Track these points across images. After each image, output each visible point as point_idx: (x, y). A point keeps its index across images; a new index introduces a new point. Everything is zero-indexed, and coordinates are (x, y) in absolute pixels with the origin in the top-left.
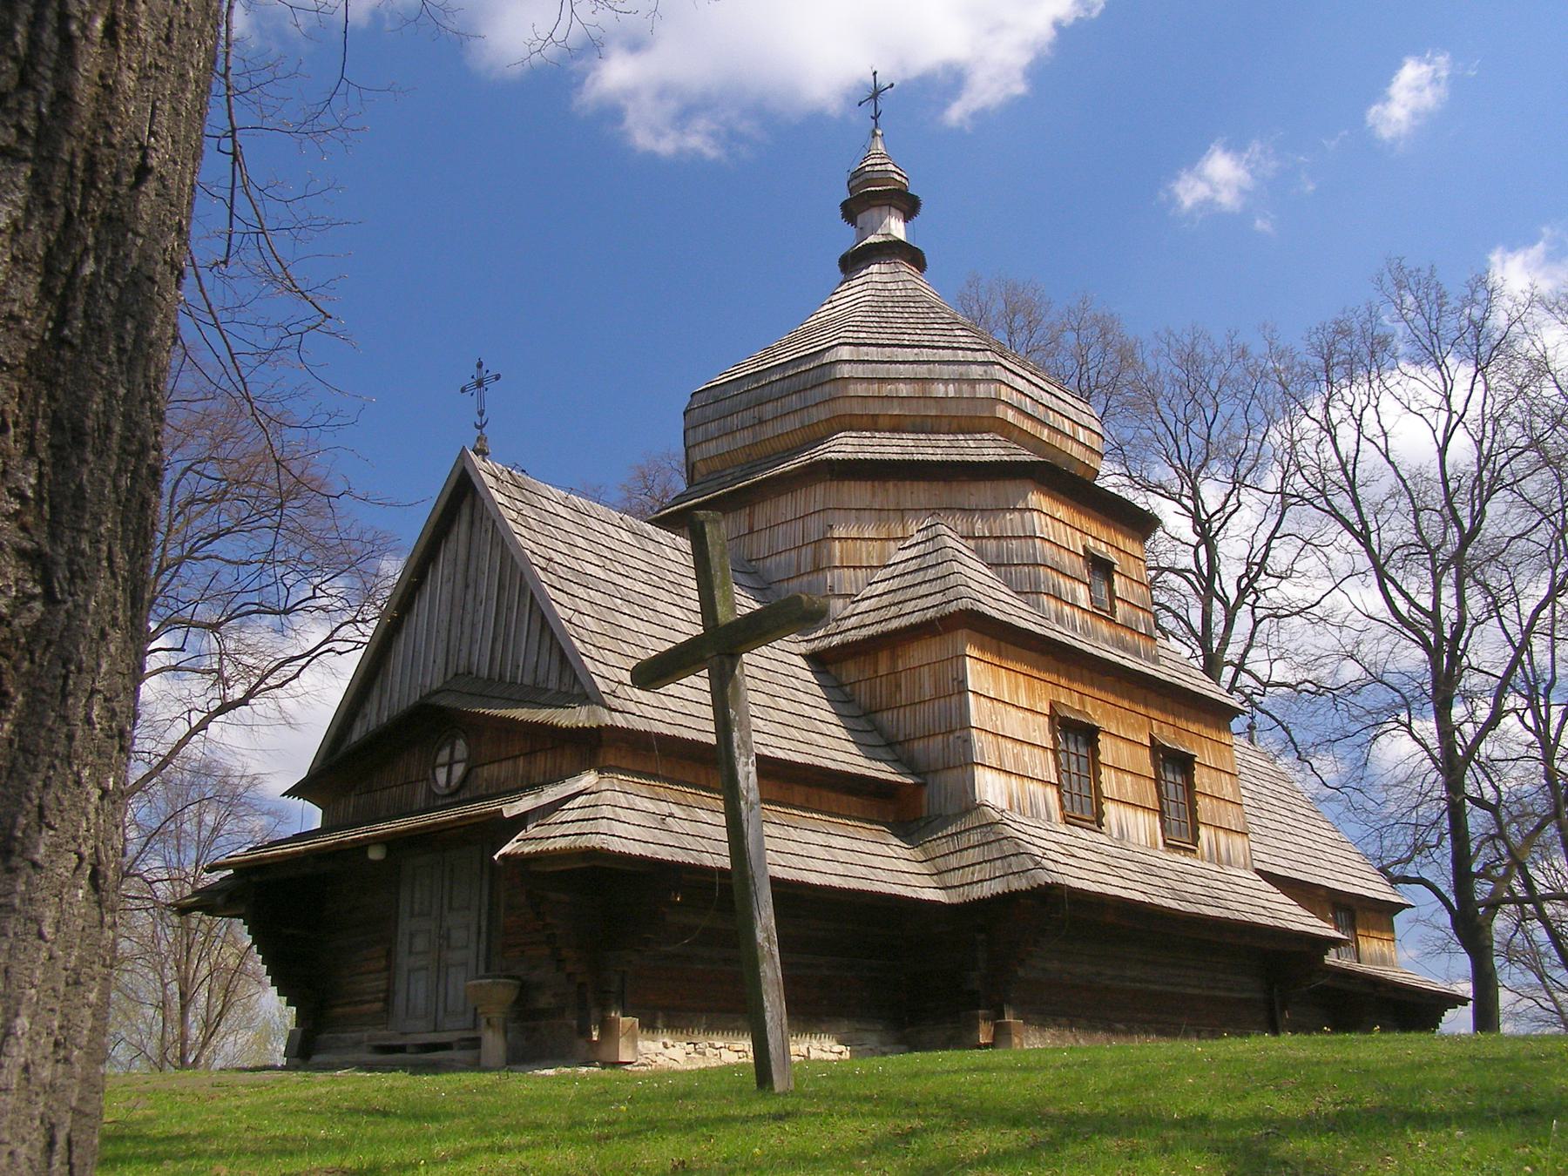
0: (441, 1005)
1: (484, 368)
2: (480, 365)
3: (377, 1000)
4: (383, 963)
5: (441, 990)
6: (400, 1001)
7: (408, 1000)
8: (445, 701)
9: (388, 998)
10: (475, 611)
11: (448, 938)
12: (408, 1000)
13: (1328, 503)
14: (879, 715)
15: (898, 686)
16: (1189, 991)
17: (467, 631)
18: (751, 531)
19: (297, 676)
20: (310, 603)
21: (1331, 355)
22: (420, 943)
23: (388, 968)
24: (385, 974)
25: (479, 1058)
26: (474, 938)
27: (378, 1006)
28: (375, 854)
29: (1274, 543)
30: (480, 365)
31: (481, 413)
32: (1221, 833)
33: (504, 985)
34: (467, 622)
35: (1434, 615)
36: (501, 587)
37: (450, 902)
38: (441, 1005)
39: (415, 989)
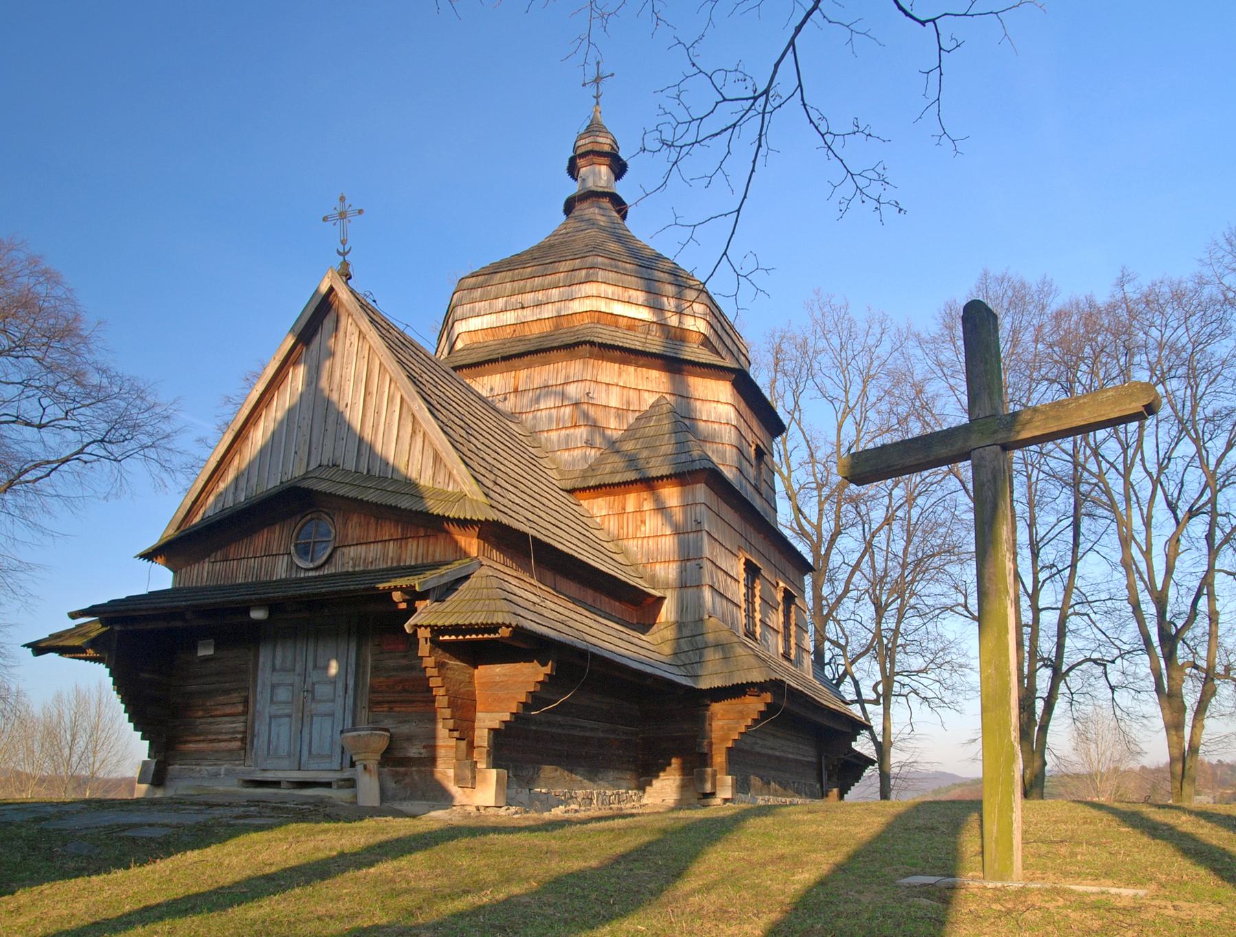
1: (347, 203)
2: (342, 199)
3: (235, 739)
4: (240, 708)
6: (261, 742)
7: (269, 742)
8: (305, 484)
9: (246, 739)
11: (313, 692)
12: (269, 742)
14: (625, 542)
15: (643, 522)
16: (791, 756)
18: (1113, 689)
19: (48, 475)
20: (62, 422)
22: (283, 694)
23: (245, 713)
24: (242, 718)
25: (356, 796)
26: (340, 692)
27: (236, 745)
28: (257, 614)
30: (342, 199)
31: (344, 243)
33: (380, 736)
35: (818, 527)
36: (367, 393)
39: (275, 729)
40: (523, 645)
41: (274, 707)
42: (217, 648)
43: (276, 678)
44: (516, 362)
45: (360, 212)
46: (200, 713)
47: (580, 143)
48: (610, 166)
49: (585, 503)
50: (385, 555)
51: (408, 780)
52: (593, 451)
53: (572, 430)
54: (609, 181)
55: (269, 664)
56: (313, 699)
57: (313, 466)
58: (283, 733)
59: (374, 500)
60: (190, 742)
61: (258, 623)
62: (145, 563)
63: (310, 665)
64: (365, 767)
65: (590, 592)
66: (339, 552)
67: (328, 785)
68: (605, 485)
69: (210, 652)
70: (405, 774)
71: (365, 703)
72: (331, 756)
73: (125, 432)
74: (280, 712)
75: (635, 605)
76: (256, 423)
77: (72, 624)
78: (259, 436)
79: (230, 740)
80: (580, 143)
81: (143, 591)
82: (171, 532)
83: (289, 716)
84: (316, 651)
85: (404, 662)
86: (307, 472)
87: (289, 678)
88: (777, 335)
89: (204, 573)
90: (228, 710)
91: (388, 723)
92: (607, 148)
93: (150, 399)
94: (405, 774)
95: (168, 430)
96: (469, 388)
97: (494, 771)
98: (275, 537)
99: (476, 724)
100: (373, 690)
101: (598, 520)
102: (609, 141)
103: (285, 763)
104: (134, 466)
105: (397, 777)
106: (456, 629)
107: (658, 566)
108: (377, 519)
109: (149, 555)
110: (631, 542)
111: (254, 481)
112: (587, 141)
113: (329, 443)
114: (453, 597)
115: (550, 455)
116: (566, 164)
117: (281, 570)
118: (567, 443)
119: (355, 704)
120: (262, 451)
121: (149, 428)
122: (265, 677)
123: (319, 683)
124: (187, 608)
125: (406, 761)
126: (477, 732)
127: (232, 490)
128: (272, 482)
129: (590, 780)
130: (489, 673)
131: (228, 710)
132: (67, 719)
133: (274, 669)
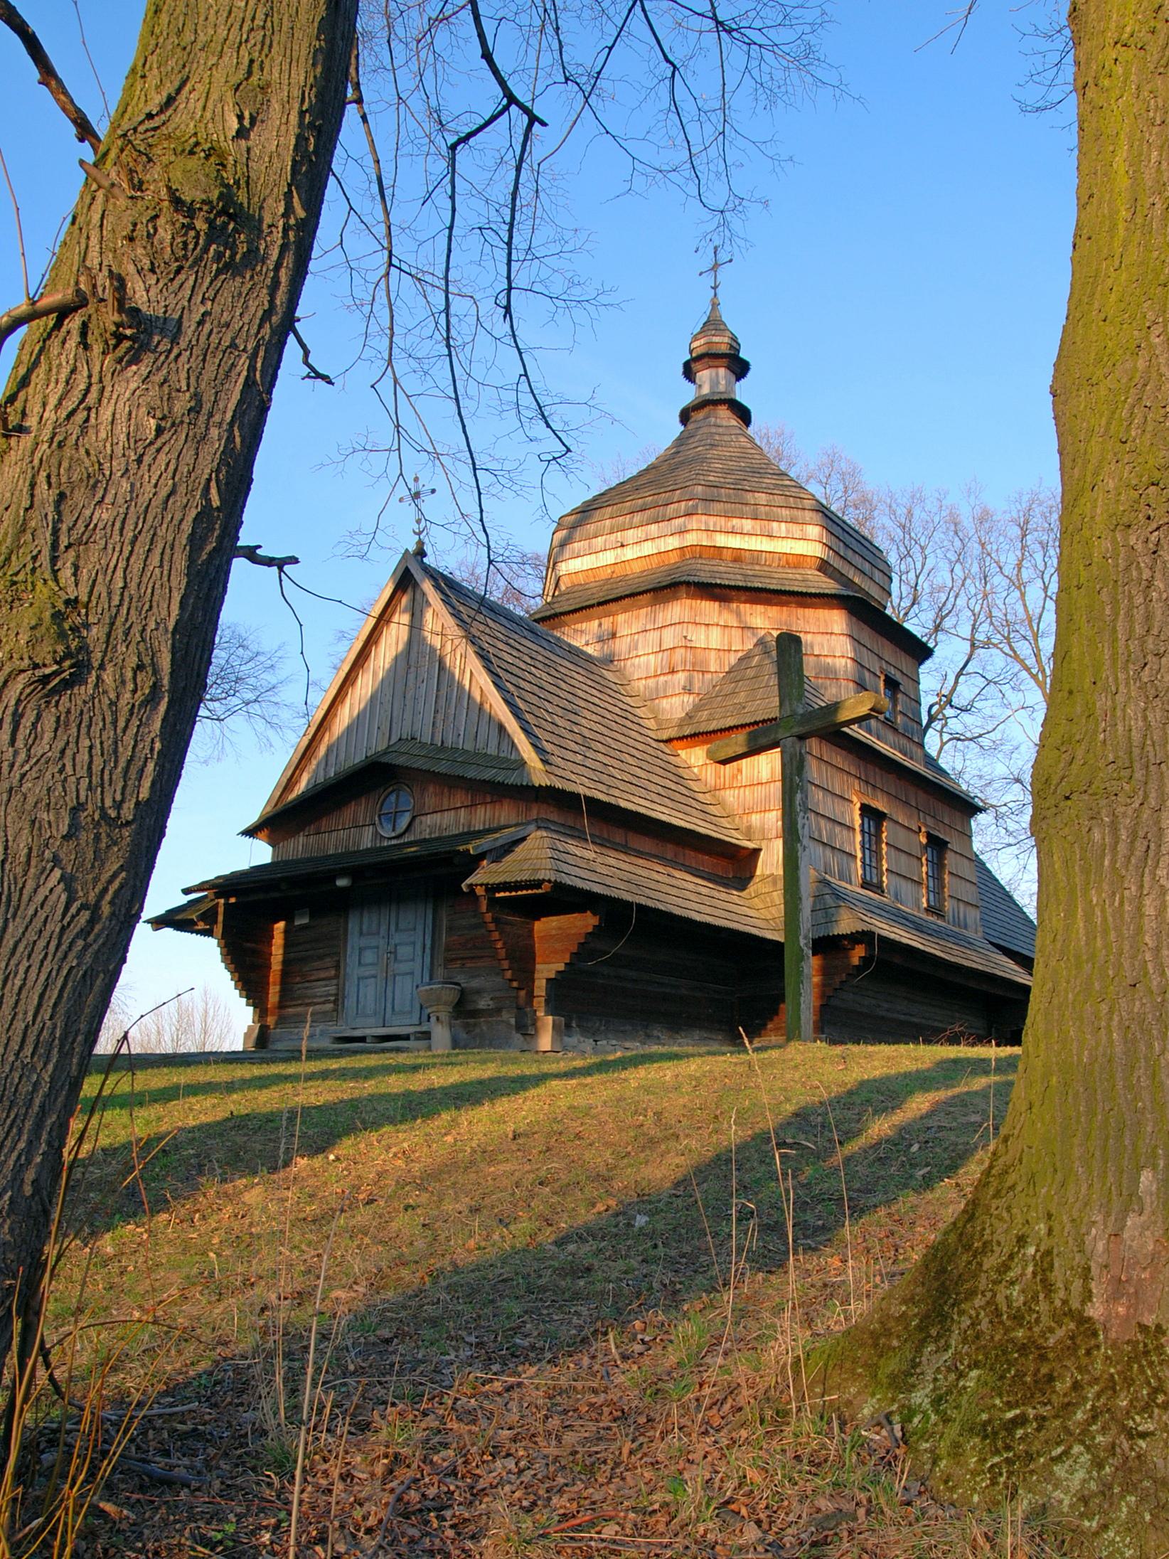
0: (389, 1006)
1: (421, 483)
3: (328, 1001)
4: (333, 972)
5: (389, 994)
6: (350, 1003)
8: (385, 760)
9: (338, 1000)
10: (417, 688)
11: (395, 953)
13: (1012, 649)
14: (722, 792)
17: (409, 703)
21: (1026, 522)
22: (369, 957)
23: (337, 976)
24: (335, 982)
27: (330, 1006)
28: (342, 882)
29: (962, 679)
32: (962, 906)
34: (410, 695)
37: (397, 924)
38: (389, 1006)
40: (564, 899)
41: (362, 969)
42: (311, 917)
43: (364, 942)
44: (613, 607)
45: (433, 491)
46: (298, 979)
47: (694, 345)
48: (728, 368)
49: (682, 753)
50: (457, 822)
51: (478, 1030)
52: (692, 697)
53: (670, 676)
54: (728, 383)
55: (357, 928)
56: (396, 959)
57: (394, 739)
58: (369, 992)
59: (444, 771)
60: (290, 1006)
61: (343, 889)
62: (247, 840)
63: (393, 928)
64: (438, 1019)
65: (669, 846)
66: (417, 820)
67: (407, 1038)
68: (702, 734)
69: (305, 921)
70: (475, 1025)
71: (441, 961)
72: (411, 1012)
73: (227, 686)
74: (367, 973)
75: (733, 864)
76: (343, 701)
77: (184, 899)
78: (365, 686)
79: (324, 1003)
80: (694, 345)
81: (244, 866)
82: (269, 809)
83: (375, 977)
84: (398, 914)
85: (473, 921)
86: (389, 747)
87: (373, 941)
88: (1025, 498)
89: (299, 846)
90: (323, 975)
91: (460, 978)
92: (724, 349)
93: (254, 648)
94: (475, 1025)
95: (274, 681)
96: (559, 643)
97: (550, 1018)
98: (358, 810)
99: (536, 976)
100: (448, 949)
101: (696, 770)
102: (726, 340)
103: (372, 1021)
104: (236, 722)
105: (468, 1029)
106: (505, 886)
107: (754, 816)
108: (450, 788)
109: (251, 832)
110: (728, 792)
111: (342, 756)
112: (702, 341)
113: (408, 716)
114: (509, 858)
115: (648, 703)
116: (681, 370)
117: (367, 842)
118: (665, 690)
119: (432, 963)
120: (349, 728)
121: (251, 681)
122: (354, 941)
123: (400, 944)
124: (282, 879)
125: (475, 1013)
126: (537, 983)
127: (323, 766)
128: (358, 758)
129: (670, 1037)
130: (545, 926)
131: (323, 975)
132: (167, 1038)
133: (361, 933)
